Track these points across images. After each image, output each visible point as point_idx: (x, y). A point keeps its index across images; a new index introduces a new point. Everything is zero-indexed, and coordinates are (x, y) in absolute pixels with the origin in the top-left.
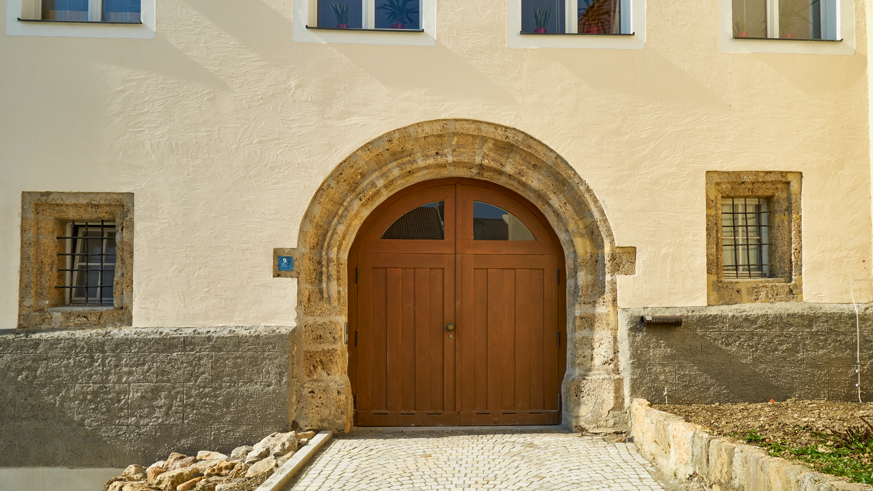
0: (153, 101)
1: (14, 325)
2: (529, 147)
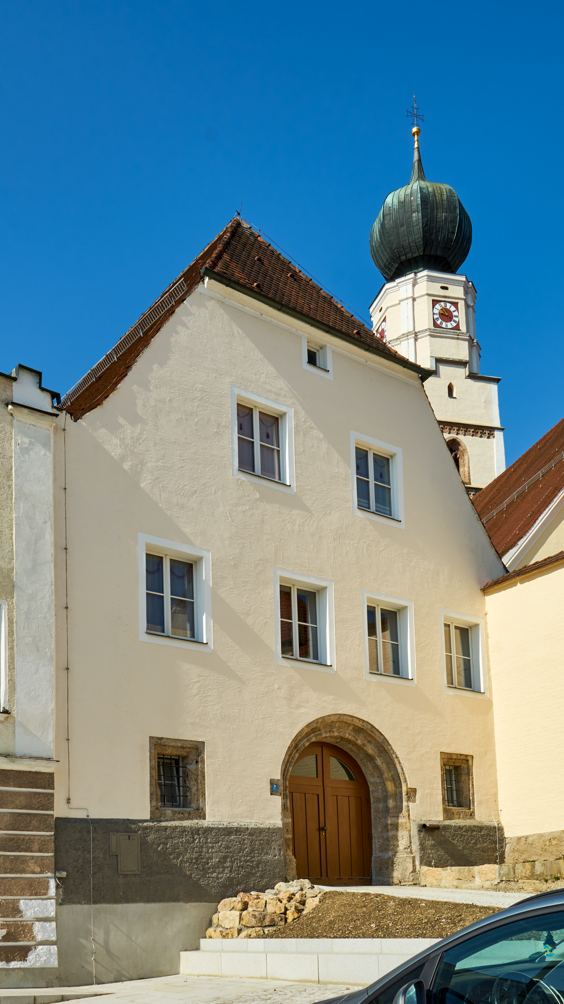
0: (213, 689)
1: (148, 817)
2: (372, 732)
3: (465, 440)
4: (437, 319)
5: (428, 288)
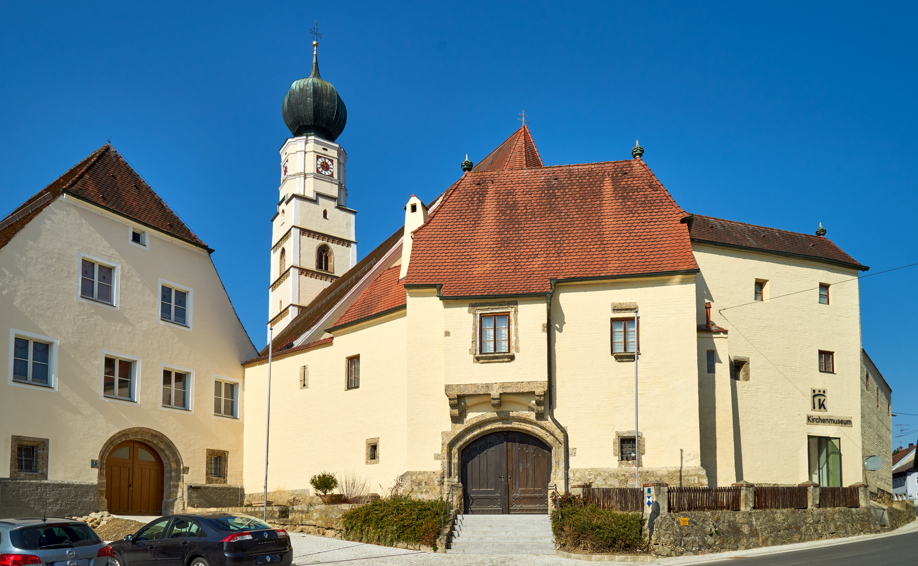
3: (333, 246)
5: (314, 148)
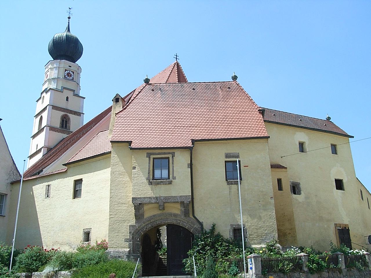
3: (70, 116)
4: (66, 75)
